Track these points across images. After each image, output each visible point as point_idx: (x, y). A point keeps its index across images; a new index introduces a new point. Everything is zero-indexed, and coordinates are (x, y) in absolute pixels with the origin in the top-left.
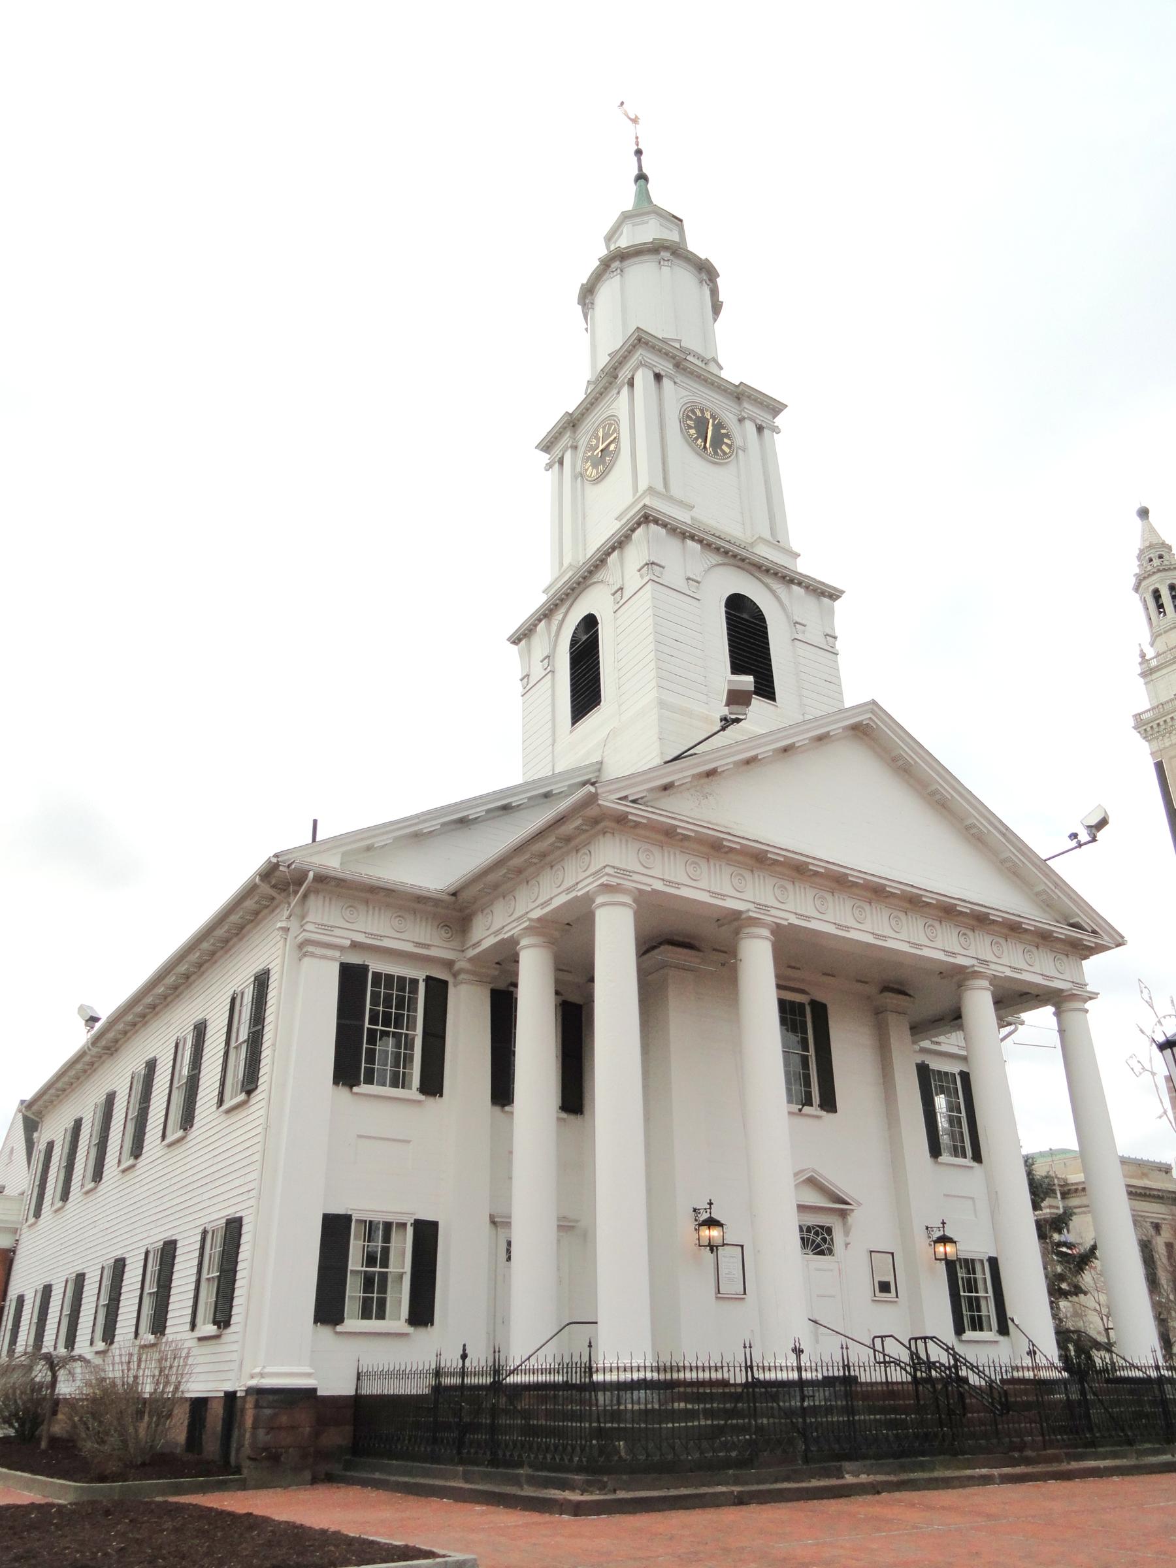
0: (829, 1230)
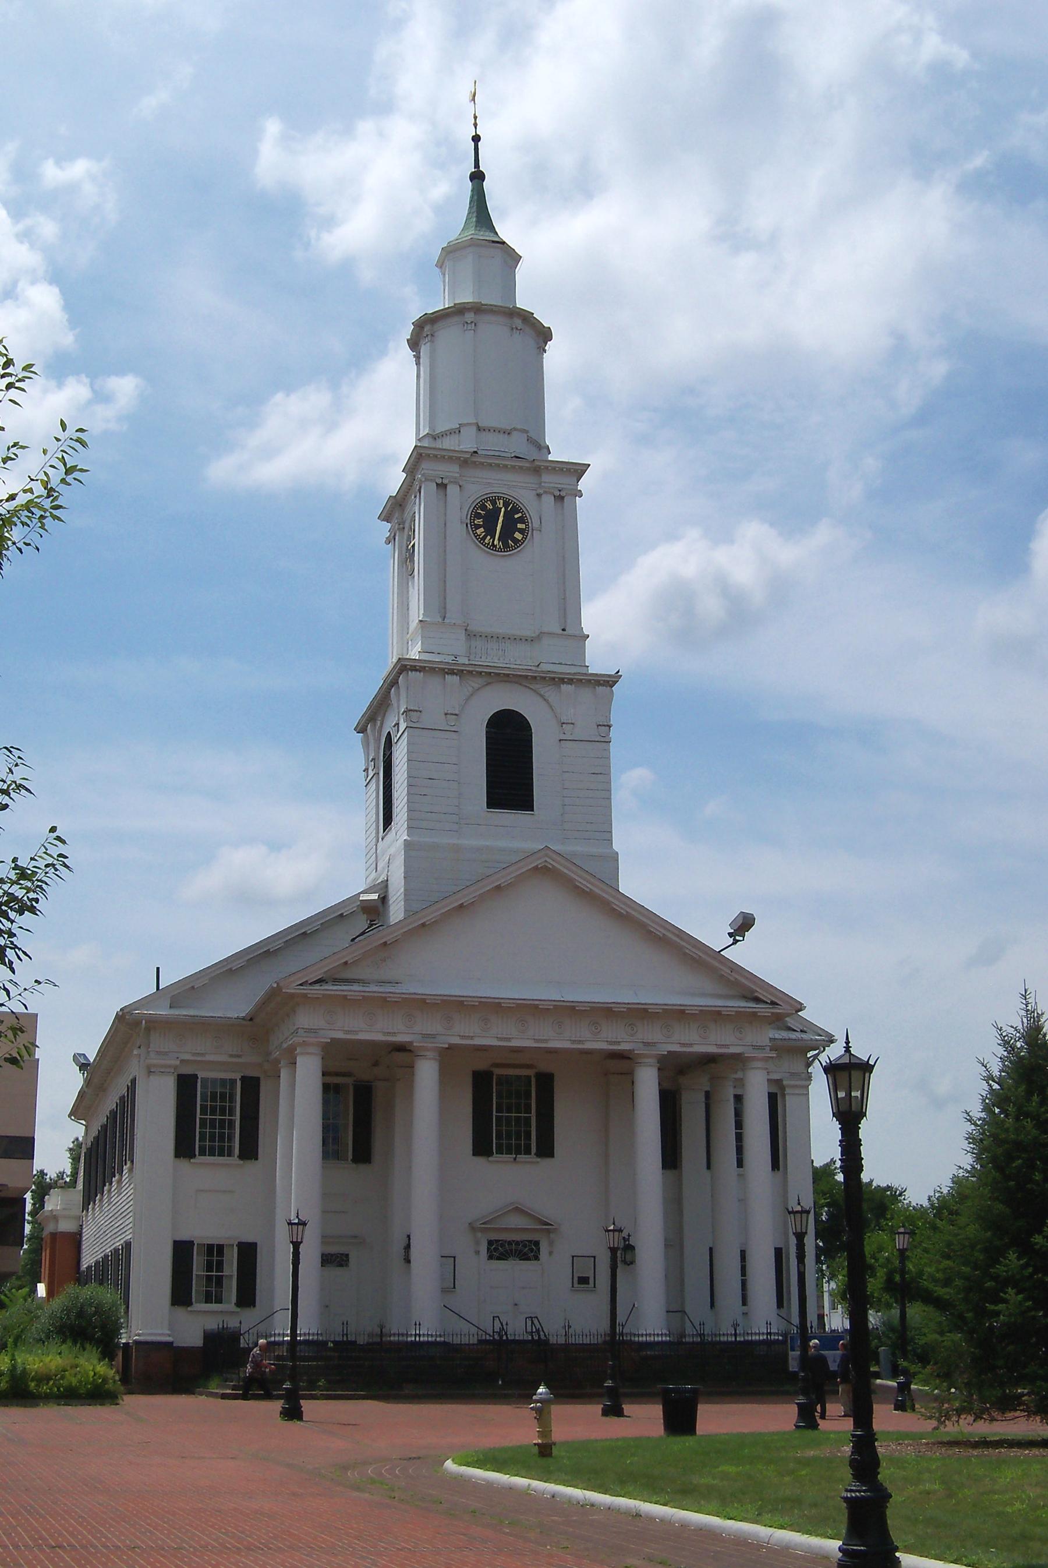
0: (537, 1243)
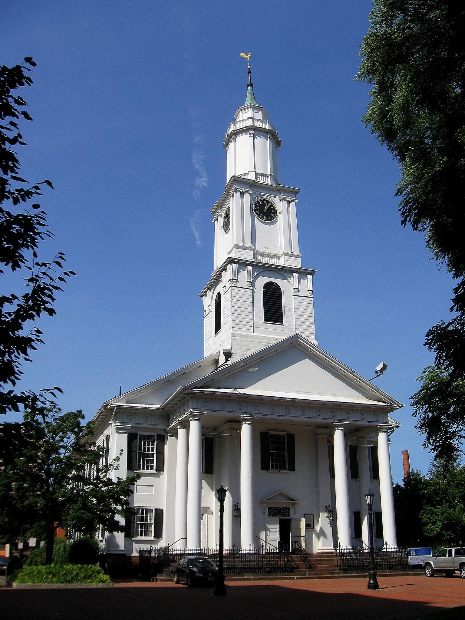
0: (289, 509)
